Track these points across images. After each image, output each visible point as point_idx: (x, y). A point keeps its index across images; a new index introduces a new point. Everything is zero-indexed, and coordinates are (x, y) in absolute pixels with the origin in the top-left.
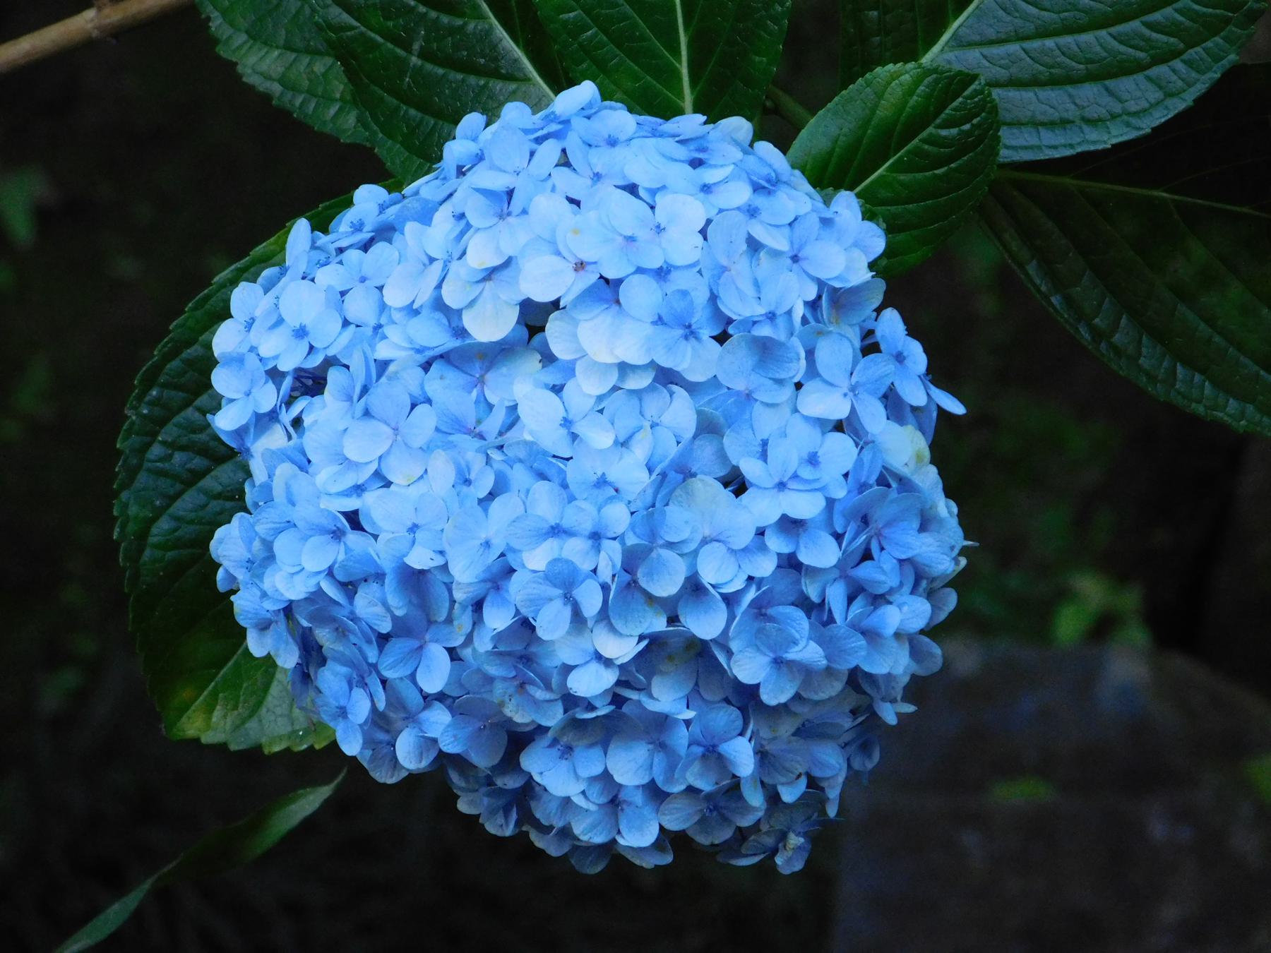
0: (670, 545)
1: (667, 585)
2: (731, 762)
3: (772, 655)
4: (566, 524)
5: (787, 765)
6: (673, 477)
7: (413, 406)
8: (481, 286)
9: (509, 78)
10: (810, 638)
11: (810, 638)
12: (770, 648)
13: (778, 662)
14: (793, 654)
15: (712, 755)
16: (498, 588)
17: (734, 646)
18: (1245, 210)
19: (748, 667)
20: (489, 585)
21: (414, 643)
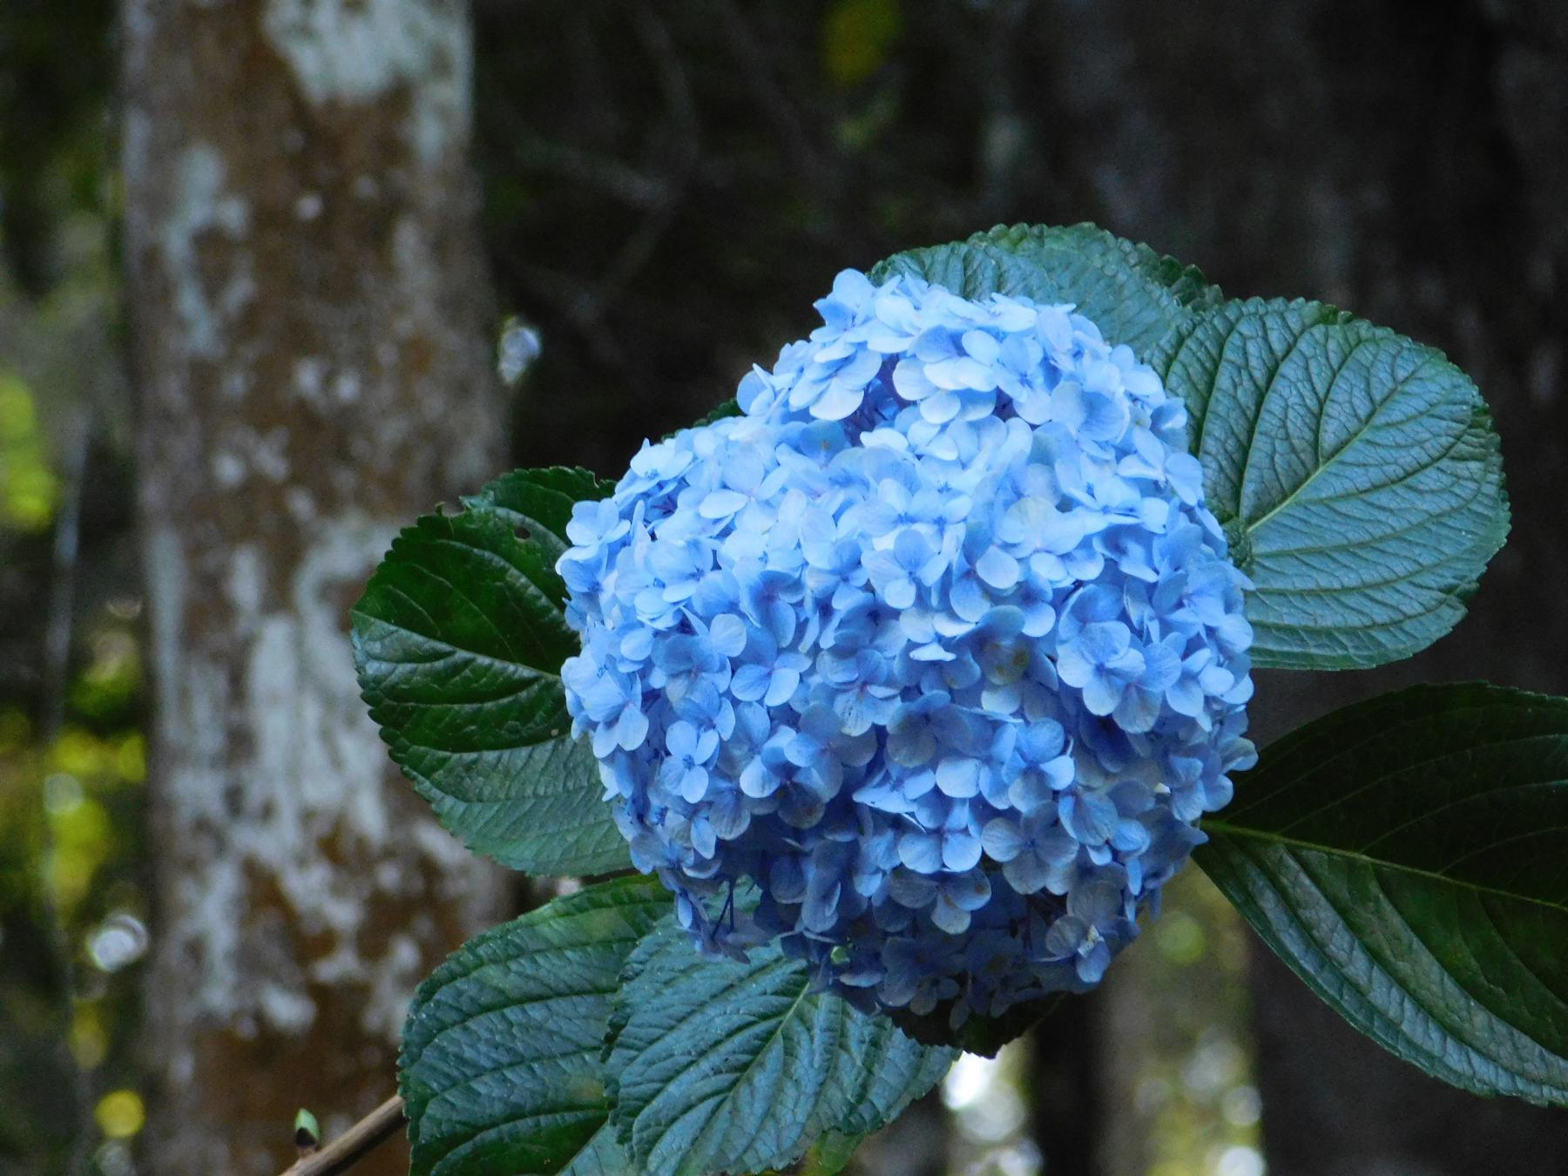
0: (1007, 547)
1: (1004, 577)
2: (1050, 777)
3: (1094, 662)
4: (911, 513)
5: (1096, 822)
6: (1011, 492)
7: (767, 472)
8: (823, 386)
9: (734, 821)
10: (1131, 646)
11: (1131, 646)
12: (1093, 653)
13: (1101, 670)
14: (1112, 664)
15: (1033, 772)
16: (846, 580)
17: (1061, 651)
18: (1436, 875)
19: (1073, 671)
20: (837, 578)
21: (763, 670)
